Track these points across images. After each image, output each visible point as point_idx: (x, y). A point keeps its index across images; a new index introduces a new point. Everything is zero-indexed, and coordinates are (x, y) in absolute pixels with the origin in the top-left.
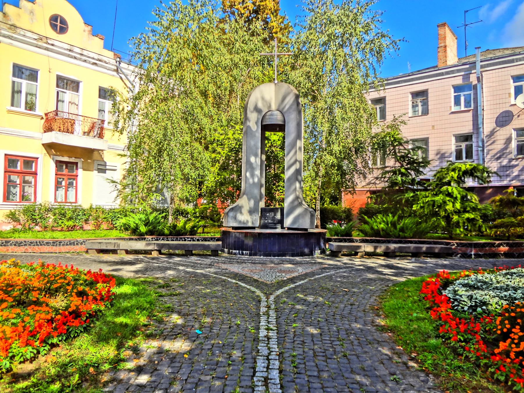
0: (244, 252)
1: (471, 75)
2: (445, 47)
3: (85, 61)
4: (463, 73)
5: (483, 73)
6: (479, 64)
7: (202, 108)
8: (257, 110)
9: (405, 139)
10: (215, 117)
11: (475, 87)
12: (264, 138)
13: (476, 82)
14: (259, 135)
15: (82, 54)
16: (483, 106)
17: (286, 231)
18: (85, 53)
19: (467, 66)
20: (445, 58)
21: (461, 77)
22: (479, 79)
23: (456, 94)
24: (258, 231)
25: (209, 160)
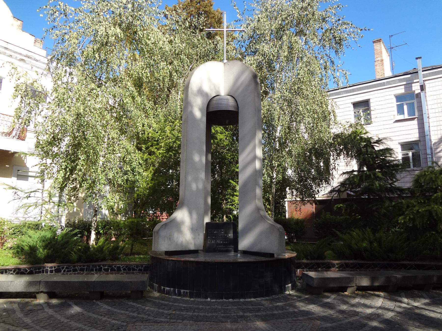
0: (182, 291)
1: (413, 85)
2: (382, 61)
3: (11, 56)
4: (405, 83)
5: (426, 82)
6: (421, 73)
7: (133, 98)
8: (200, 92)
9: (376, 139)
10: (151, 112)
11: (418, 96)
12: (210, 136)
13: (419, 91)
14: (203, 126)
15: (6, 48)
16: (428, 114)
17: (240, 258)
18: (9, 46)
19: (409, 76)
20: (382, 71)
21: (403, 87)
22: (422, 88)
23: (399, 103)
24: (201, 258)
25: (141, 162)
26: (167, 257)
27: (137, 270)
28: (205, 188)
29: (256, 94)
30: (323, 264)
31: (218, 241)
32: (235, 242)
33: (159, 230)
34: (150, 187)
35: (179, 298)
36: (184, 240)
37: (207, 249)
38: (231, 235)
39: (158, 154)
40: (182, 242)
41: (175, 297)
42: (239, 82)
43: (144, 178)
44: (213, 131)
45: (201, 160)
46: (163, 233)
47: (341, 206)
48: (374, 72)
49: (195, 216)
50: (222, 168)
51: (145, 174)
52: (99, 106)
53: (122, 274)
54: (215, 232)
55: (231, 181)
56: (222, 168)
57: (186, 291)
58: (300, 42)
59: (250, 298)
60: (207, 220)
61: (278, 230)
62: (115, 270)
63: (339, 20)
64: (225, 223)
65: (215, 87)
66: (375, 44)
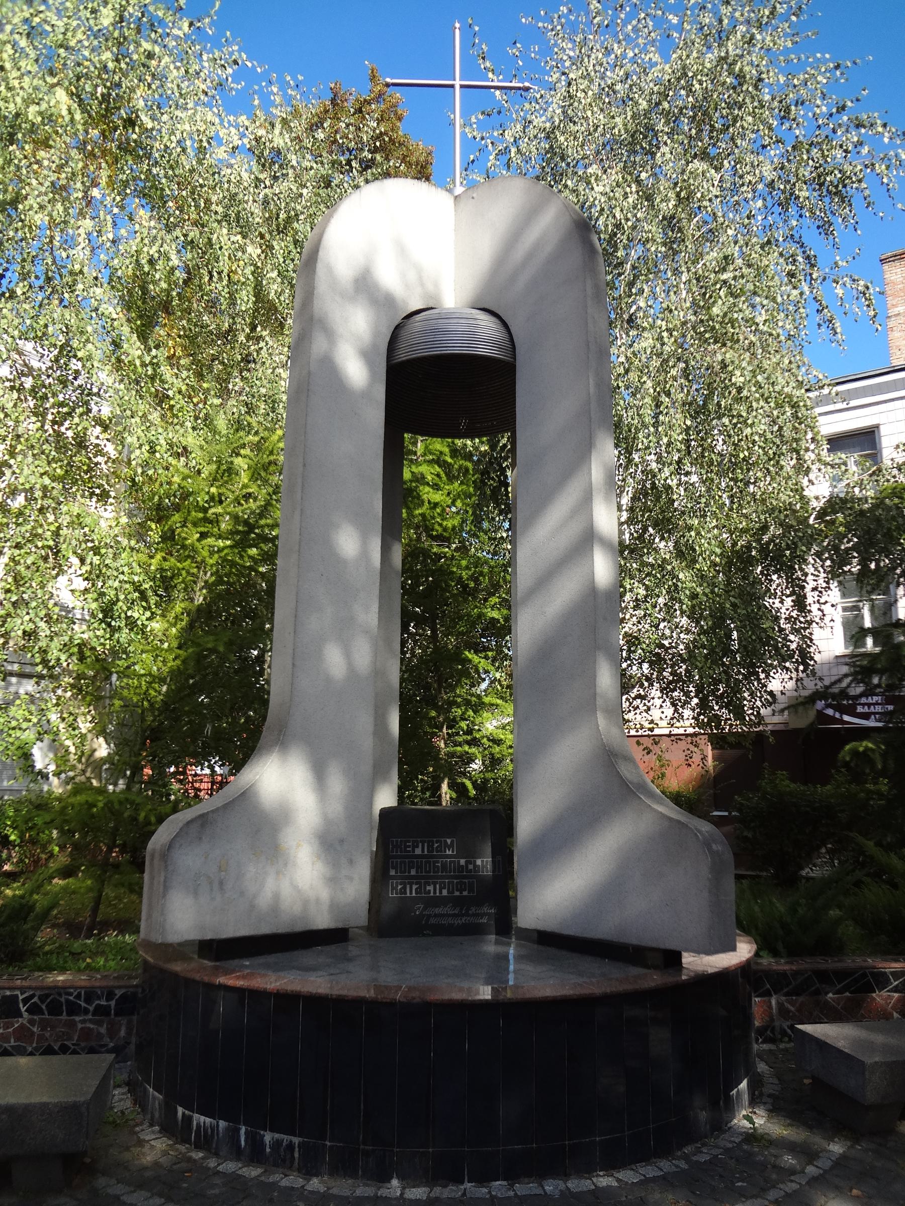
0: (268, 1137)
8: (365, 286)
12: (398, 494)
14: (374, 417)
27: (86, 1011)
28: (378, 673)
29: (590, 291)
30: (842, 975)
31: (430, 888)
32: (500, 892)
33: (171, 845)
34: (171, 672)
35: (253, 1172)
36: (286, 890)
37: (389, 923)
38: (485, 863)
39: (205, 553)
40: (277, 897)
41: (230, 1166)
42: (519, 253)
43: (155, 641)
44: (407, 475)
45: (364, 553)
46: (189, 860)
47: (867, 749)
48: (885, 347)
49: (337, 784)
50: (444, 613)
51: (156, 626)
54: (418, 851)
55: (469, 655)
56: (444, 613)
57: (286, 1138)
58: (708, 181)
59: (588, 1170)
60: (386, 797)
61: (707, 844)
63: (842, 109)
64: (445, 813)
65: (420, 278)
66: (886, 267)
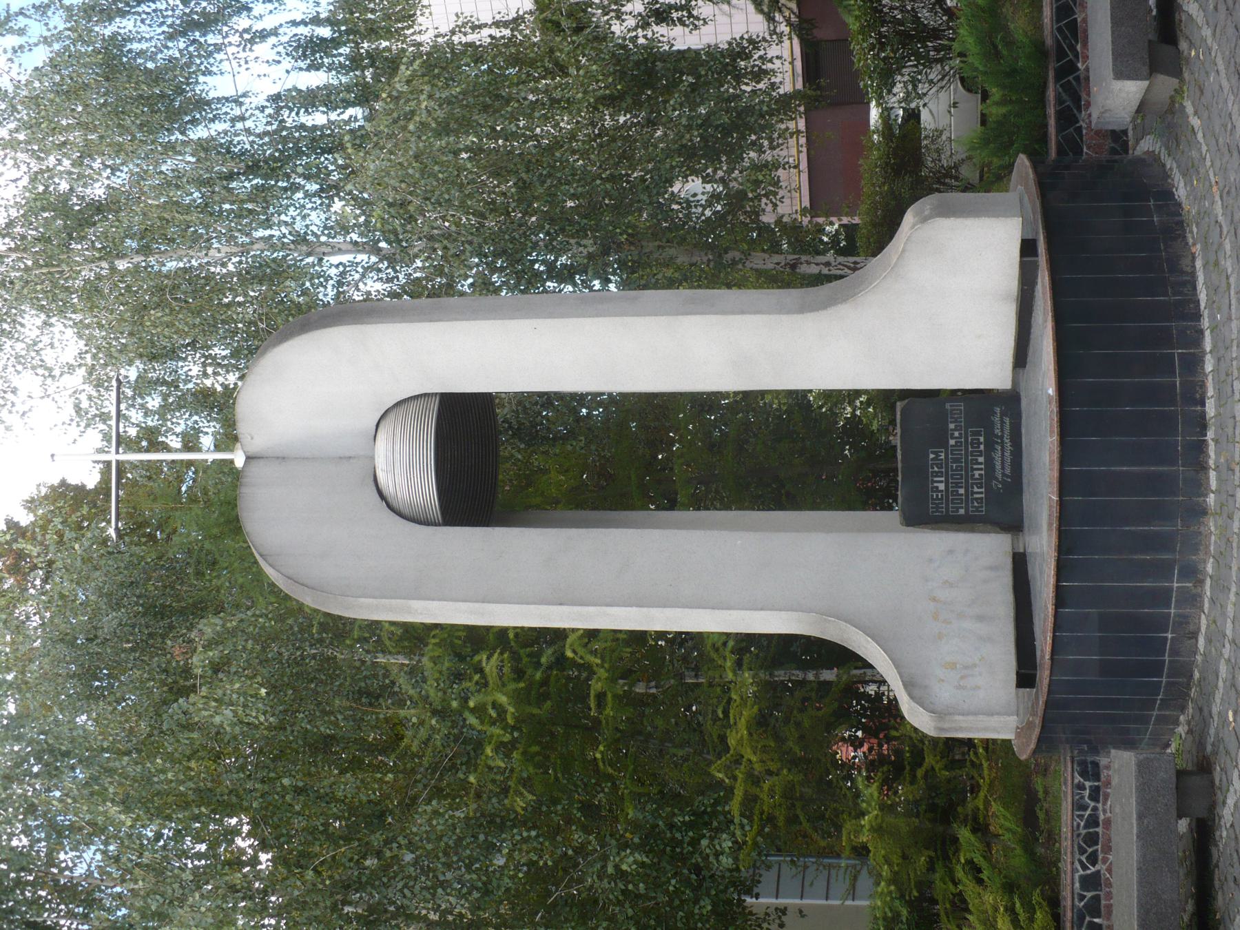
17: (1045, 382)
24: (1042, 543)
26: (1044, 676)
31: (977, 473)
52: (432, 693)
53: (1109, 870)
54: (942, 487)
61: (925, 220)
62: (1097, 899)
